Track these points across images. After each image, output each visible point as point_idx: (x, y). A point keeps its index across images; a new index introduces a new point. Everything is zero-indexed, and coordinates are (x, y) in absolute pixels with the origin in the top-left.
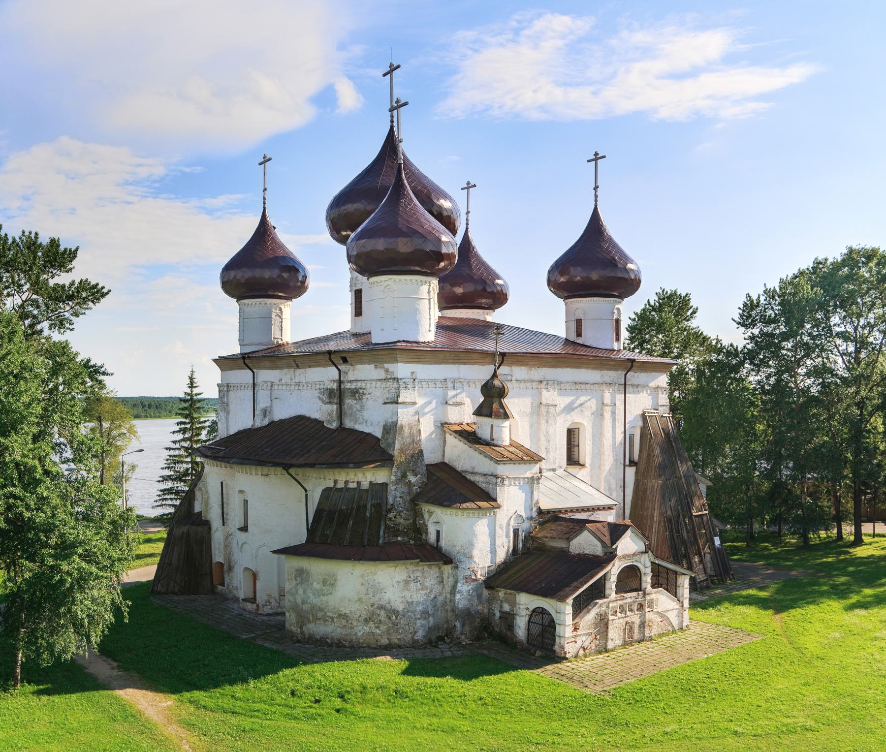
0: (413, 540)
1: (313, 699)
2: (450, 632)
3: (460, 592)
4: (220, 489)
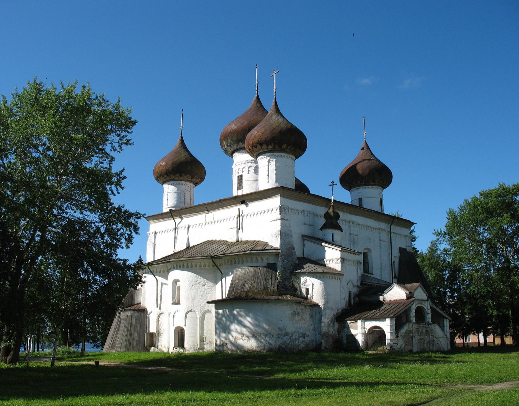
3: (324, 322)
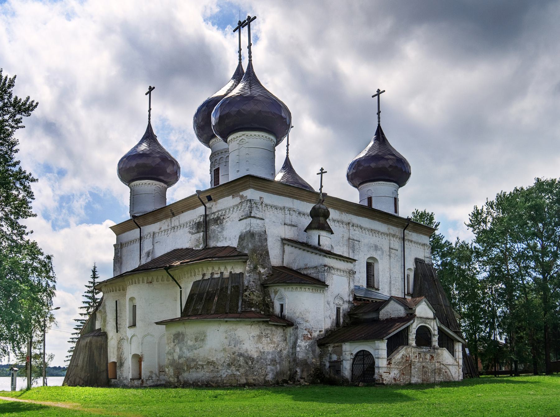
0: (263, 311)
3: (299, 346)
4: (115, 307)
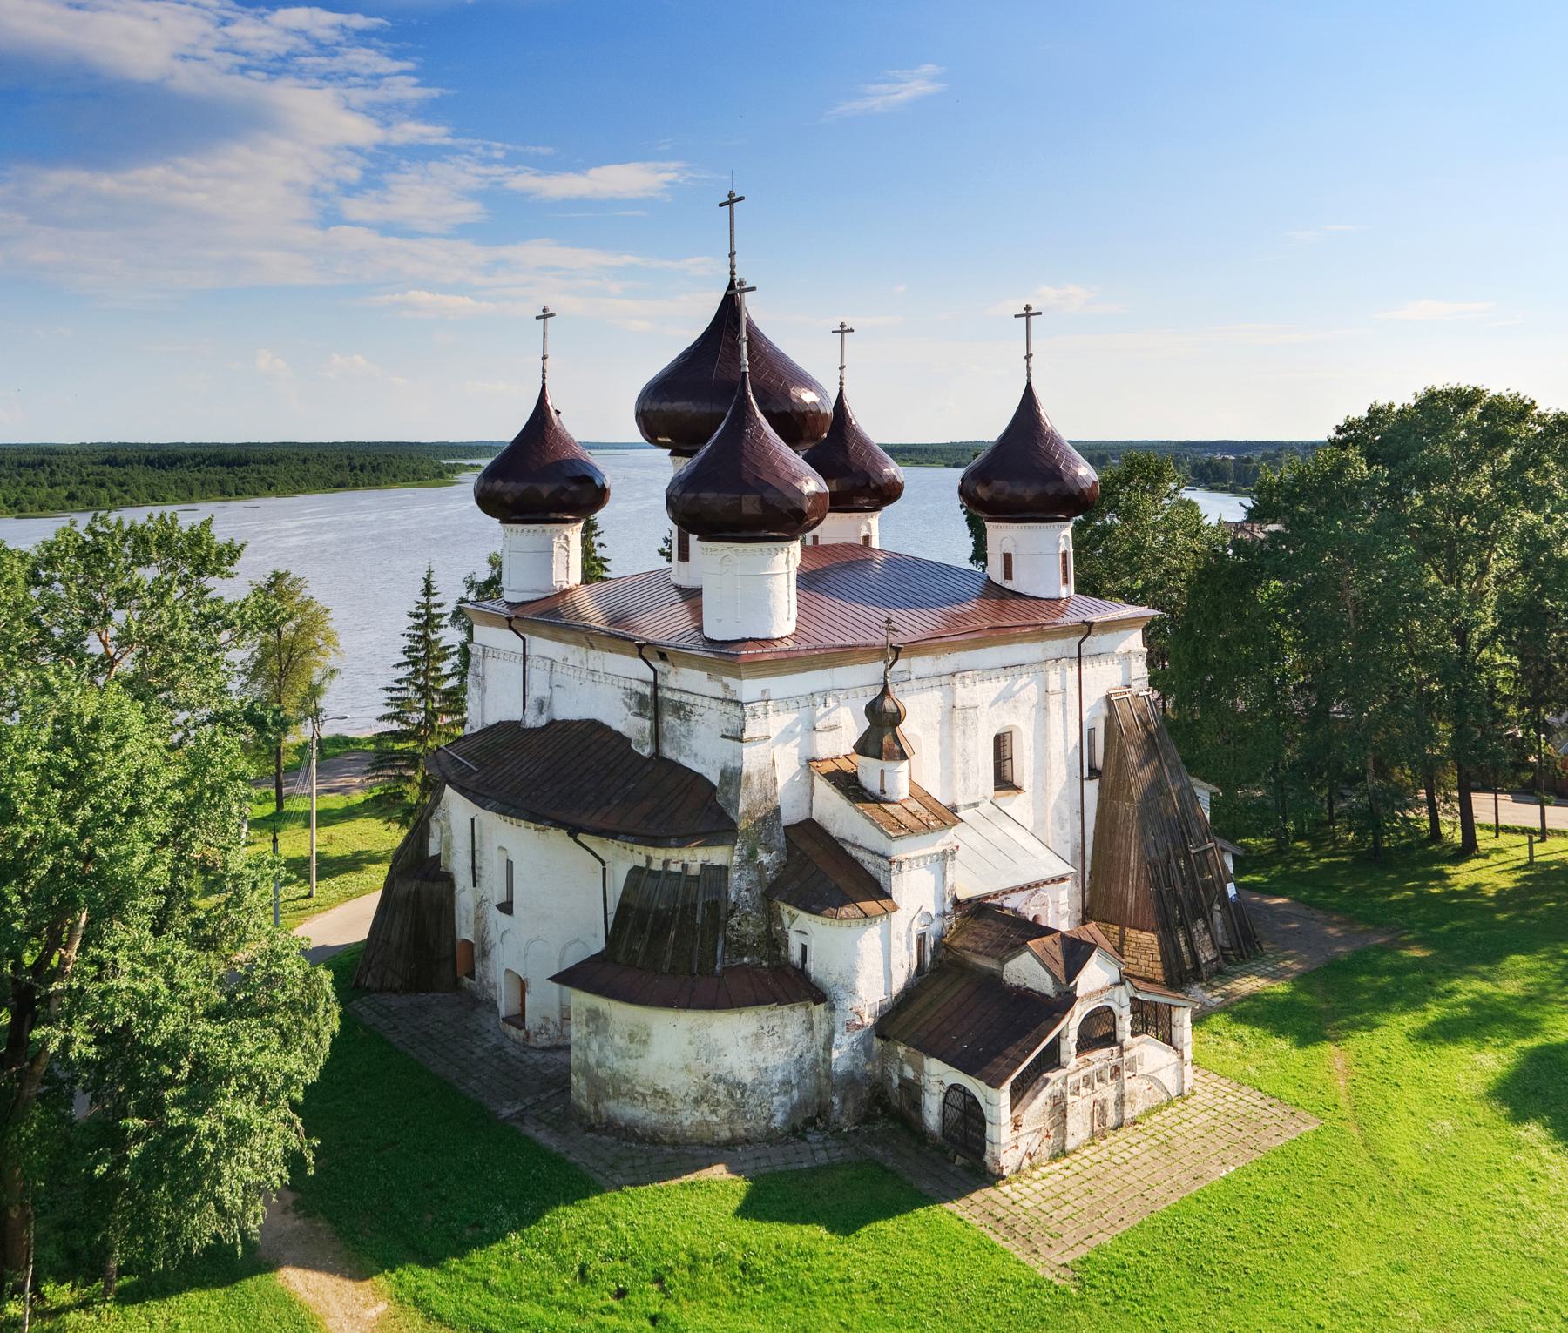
1: (613, 1287)
2: (823, 1111)
